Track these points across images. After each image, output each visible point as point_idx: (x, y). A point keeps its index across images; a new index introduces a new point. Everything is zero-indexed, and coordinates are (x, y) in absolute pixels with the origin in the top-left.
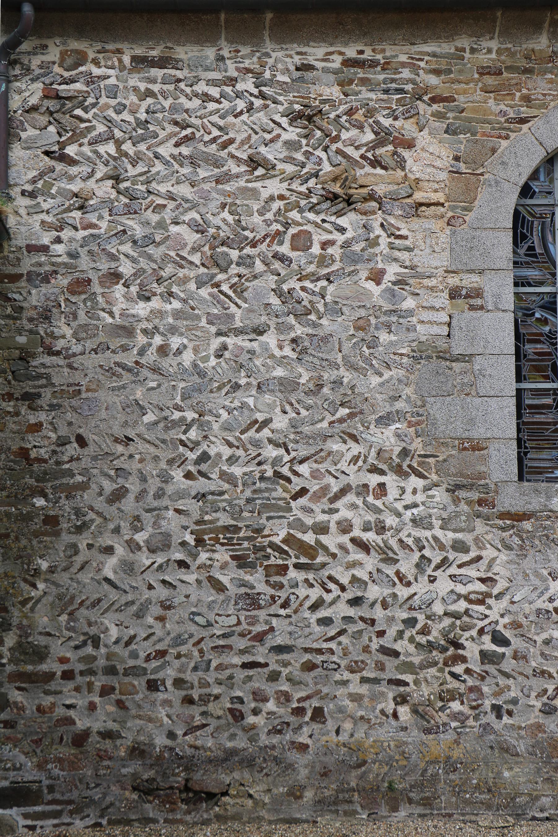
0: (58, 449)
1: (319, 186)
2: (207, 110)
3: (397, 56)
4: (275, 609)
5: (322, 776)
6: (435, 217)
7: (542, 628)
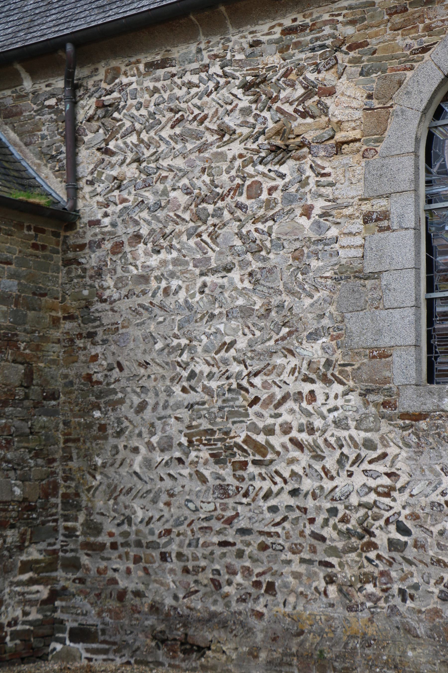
0: (108, 373)
1: (266, 142)
2: (191, 95)
3: (321, 16)
4: (239, 498)
5: (273, 640)
6: (352, 152)
7: (436, 520)
